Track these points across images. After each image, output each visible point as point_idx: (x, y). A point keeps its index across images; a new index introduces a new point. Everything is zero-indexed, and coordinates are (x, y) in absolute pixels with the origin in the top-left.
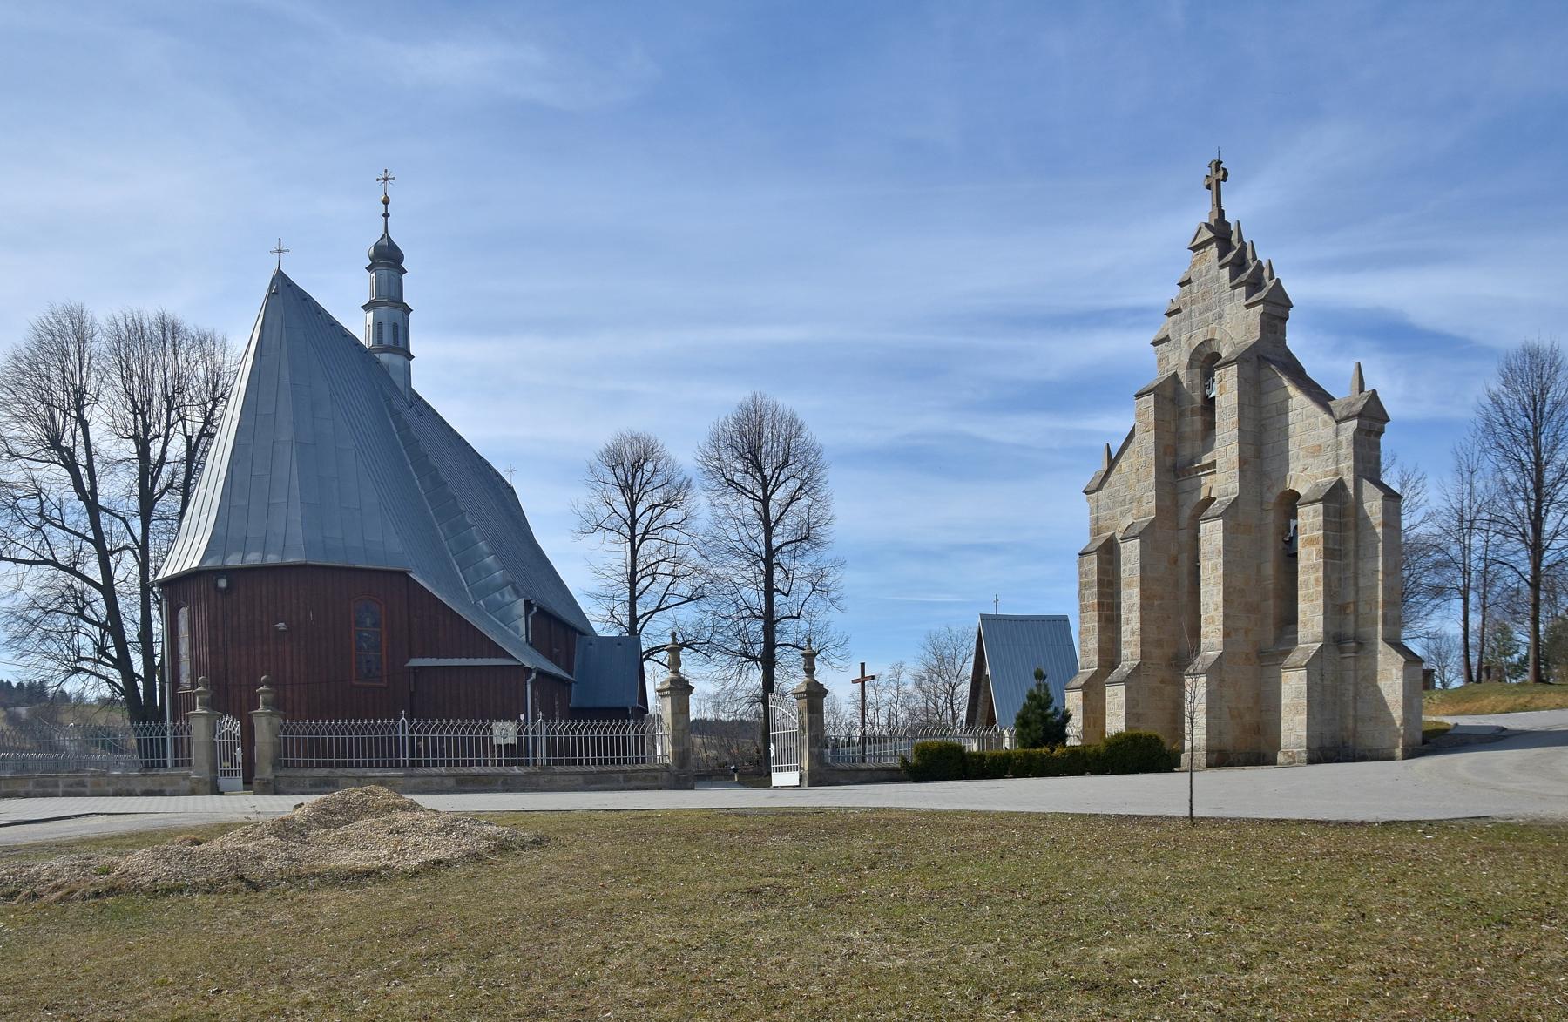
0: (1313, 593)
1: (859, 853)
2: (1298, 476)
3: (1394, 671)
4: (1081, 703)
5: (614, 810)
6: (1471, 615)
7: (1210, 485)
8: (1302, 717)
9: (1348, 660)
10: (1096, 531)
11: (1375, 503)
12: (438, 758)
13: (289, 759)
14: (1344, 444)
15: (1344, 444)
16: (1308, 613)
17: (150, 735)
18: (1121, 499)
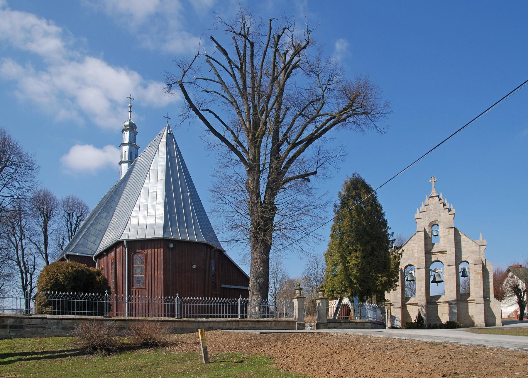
5: (294, 332)
6: (154, 290)
12: (219, 314)
13: (204, 314)
16: (478, 291)
17: (217, 304)
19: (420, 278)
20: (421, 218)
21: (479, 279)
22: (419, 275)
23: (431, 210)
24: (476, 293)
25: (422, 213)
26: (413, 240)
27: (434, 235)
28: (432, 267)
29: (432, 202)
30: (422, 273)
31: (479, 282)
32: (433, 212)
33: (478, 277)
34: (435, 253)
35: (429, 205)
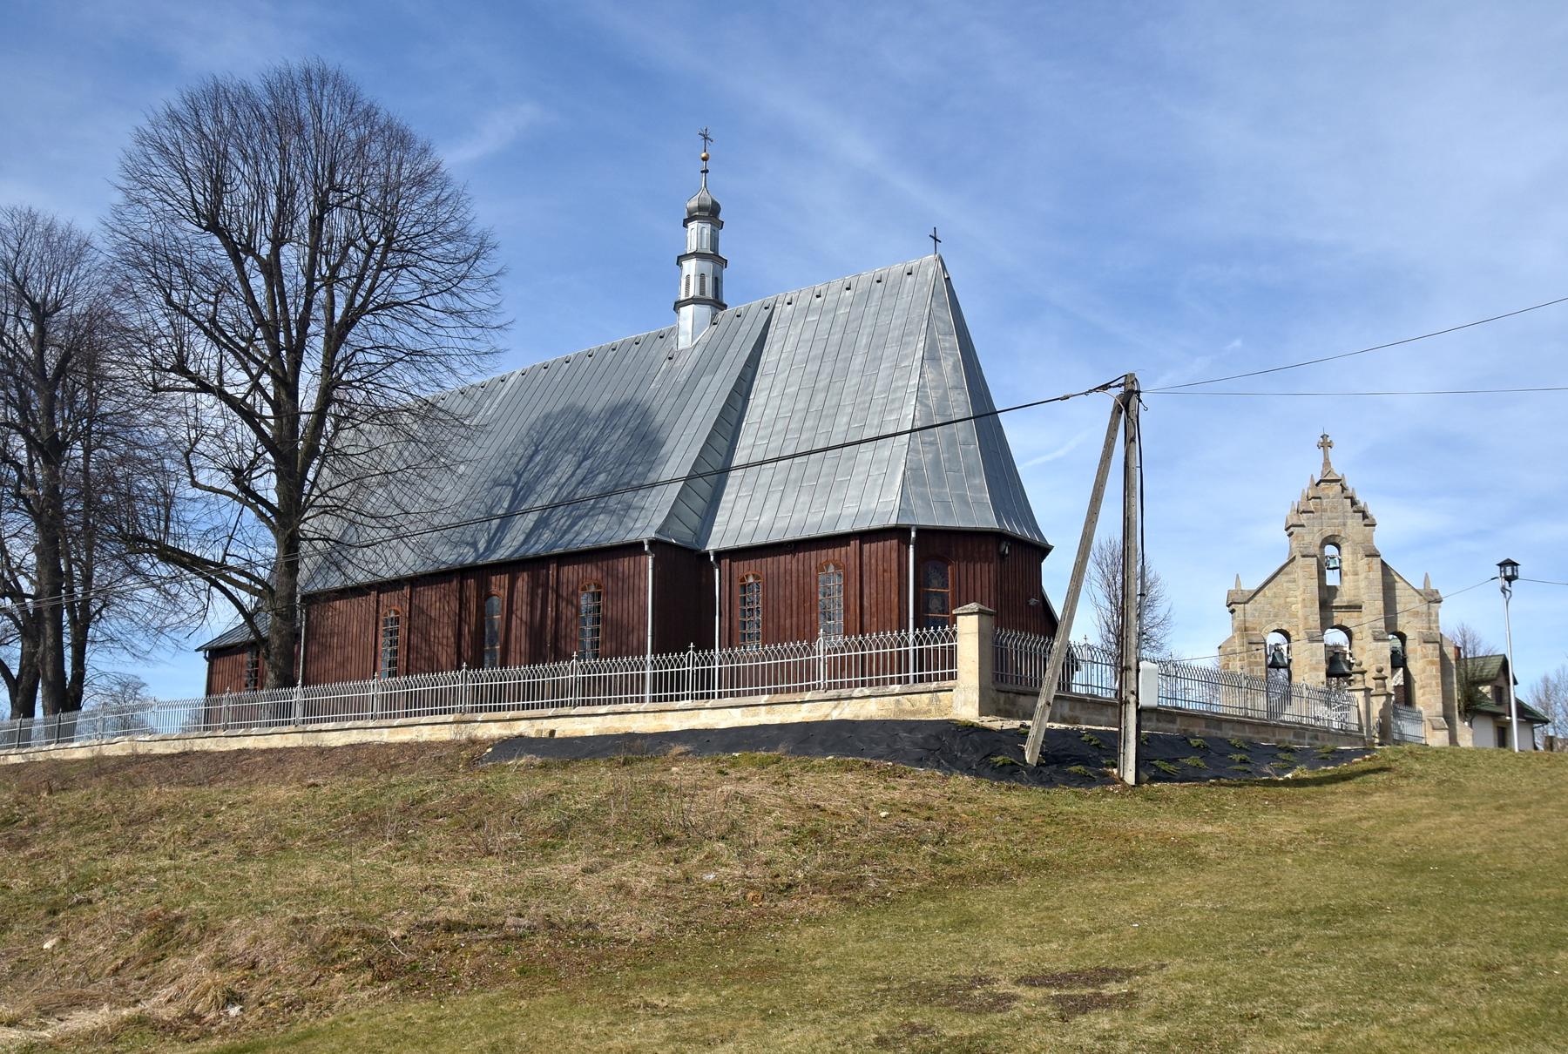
19: (1314, 662)
20: (1303, 526)
21: (1435, 676)
22: (1312, 656)
23: (1325, 510)
24: (1428, 706)
25: (1304, 515)
26: (1287, 574)
27: (1331, 566)
28: (338, 393)
29: (1326, 492)
30: (1318, 652)
31: (1434, 683)
32: (1329, 514)
33: (1431, 672)
34: (1341, 607)
35: (1320, 498)
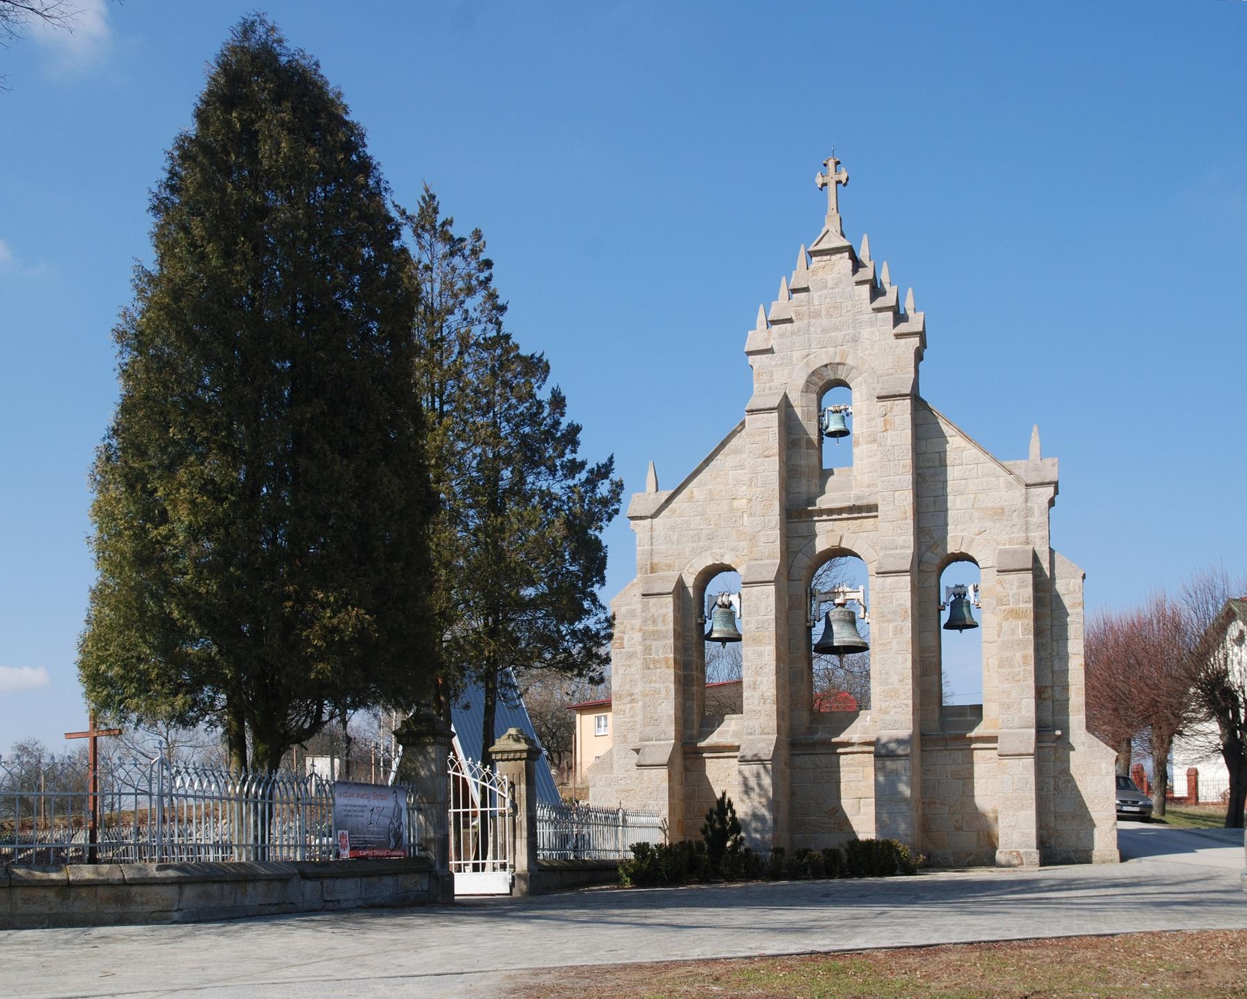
0: (1019, 672)
1: (865, 991)
2: (973, 540)
3: (1103, 765)
4: (666, 784)
7: (841, 533)
8: (1029, 812)
9: (1046, 750)
10: (649, 567)
11: (1073, 581)
14: (1037, 513)
15: (1037, 513)
18: (693, 533)
